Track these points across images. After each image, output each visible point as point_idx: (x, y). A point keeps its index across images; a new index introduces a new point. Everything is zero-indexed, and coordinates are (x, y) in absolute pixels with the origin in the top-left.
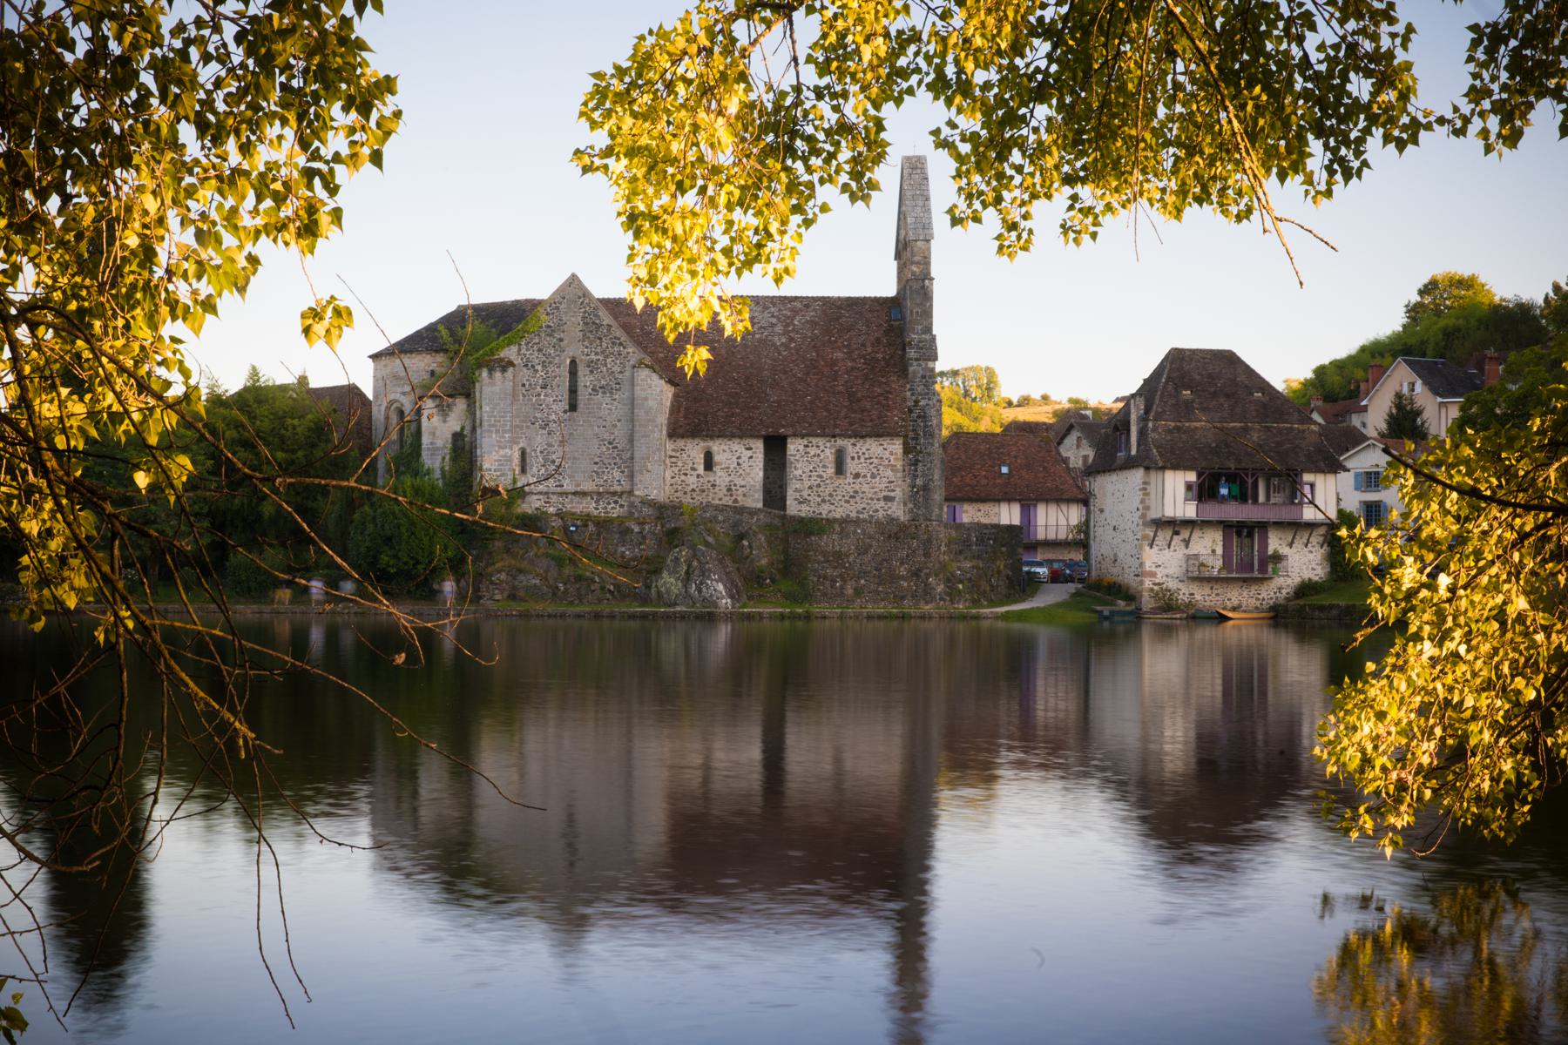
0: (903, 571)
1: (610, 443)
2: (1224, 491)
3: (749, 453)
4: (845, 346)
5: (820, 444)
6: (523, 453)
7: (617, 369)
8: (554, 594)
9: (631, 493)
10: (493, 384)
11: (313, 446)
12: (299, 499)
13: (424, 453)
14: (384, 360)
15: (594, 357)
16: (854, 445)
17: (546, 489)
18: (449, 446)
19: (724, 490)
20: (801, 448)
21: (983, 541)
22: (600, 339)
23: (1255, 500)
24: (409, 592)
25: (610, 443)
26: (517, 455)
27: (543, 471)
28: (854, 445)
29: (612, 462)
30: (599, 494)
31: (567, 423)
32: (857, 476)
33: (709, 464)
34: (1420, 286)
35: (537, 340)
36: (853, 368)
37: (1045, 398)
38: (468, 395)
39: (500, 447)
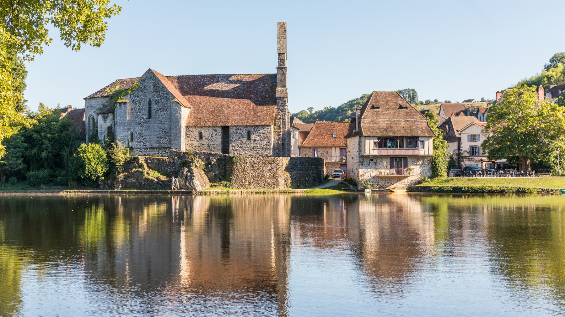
0: (268, 175)
1: (163, 130)
2: (389, 144)
3: (216, 133)
4: (255, 92)
5: (242, 129)
6: (132, 134)
7: (165, 103)
8: (140, 185)
9: (170, 148)
10: (121, 109)
11: (62, 132)
12: (56, 151)
13: (99, 134)
14: (88, 101)
15: (157, 98)
16: (254, 129)
17: (140, 147)
18: (106, 132)
19: (207, 146)
20: (235, 130)
21: (303, 164)
22: (159, 92)
23: (403, 147)
24: (91, 185)
25: (163, 130)
26: (130, 134)
27: (139, 140)
28: (254, 129)
29: (164, 136)
30: (159, 148)
31: (148, 123)
32: (255, 140)
33: (201, 137)
34: (550, 58)
35: (137, 93)
36: (257, 101)
37: (436, 101)
38: (113, 113)
39: (123, 132)
